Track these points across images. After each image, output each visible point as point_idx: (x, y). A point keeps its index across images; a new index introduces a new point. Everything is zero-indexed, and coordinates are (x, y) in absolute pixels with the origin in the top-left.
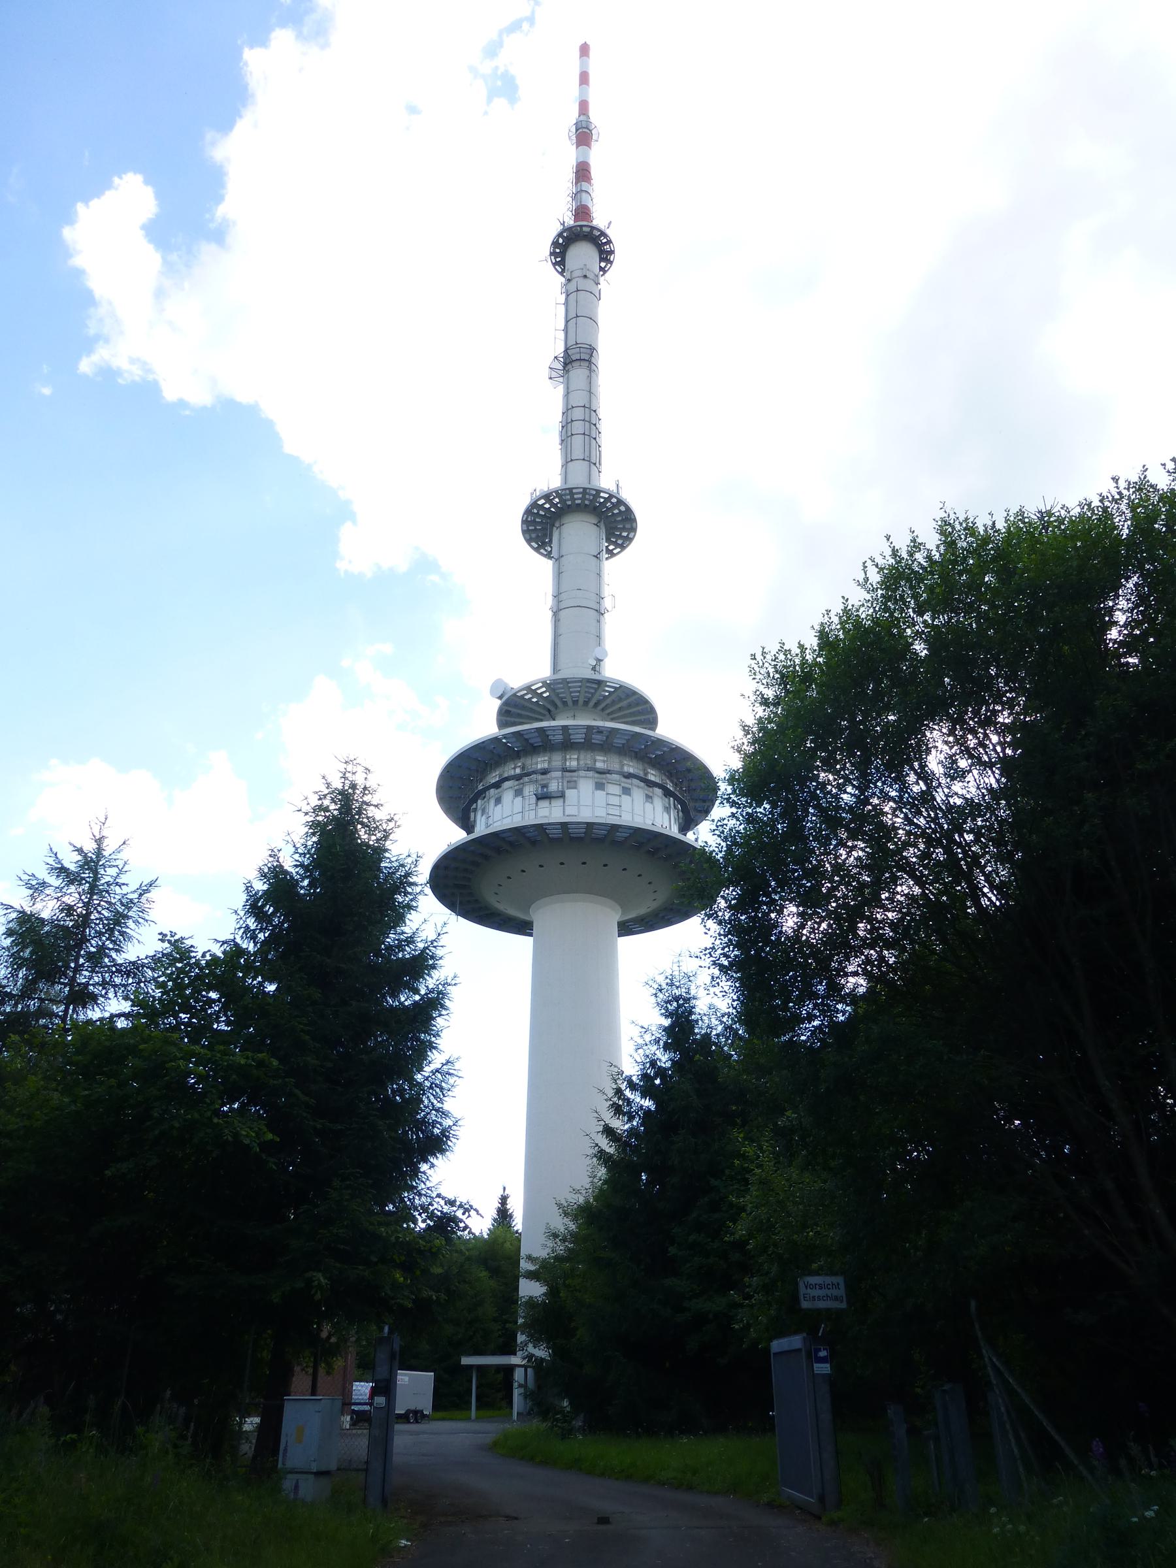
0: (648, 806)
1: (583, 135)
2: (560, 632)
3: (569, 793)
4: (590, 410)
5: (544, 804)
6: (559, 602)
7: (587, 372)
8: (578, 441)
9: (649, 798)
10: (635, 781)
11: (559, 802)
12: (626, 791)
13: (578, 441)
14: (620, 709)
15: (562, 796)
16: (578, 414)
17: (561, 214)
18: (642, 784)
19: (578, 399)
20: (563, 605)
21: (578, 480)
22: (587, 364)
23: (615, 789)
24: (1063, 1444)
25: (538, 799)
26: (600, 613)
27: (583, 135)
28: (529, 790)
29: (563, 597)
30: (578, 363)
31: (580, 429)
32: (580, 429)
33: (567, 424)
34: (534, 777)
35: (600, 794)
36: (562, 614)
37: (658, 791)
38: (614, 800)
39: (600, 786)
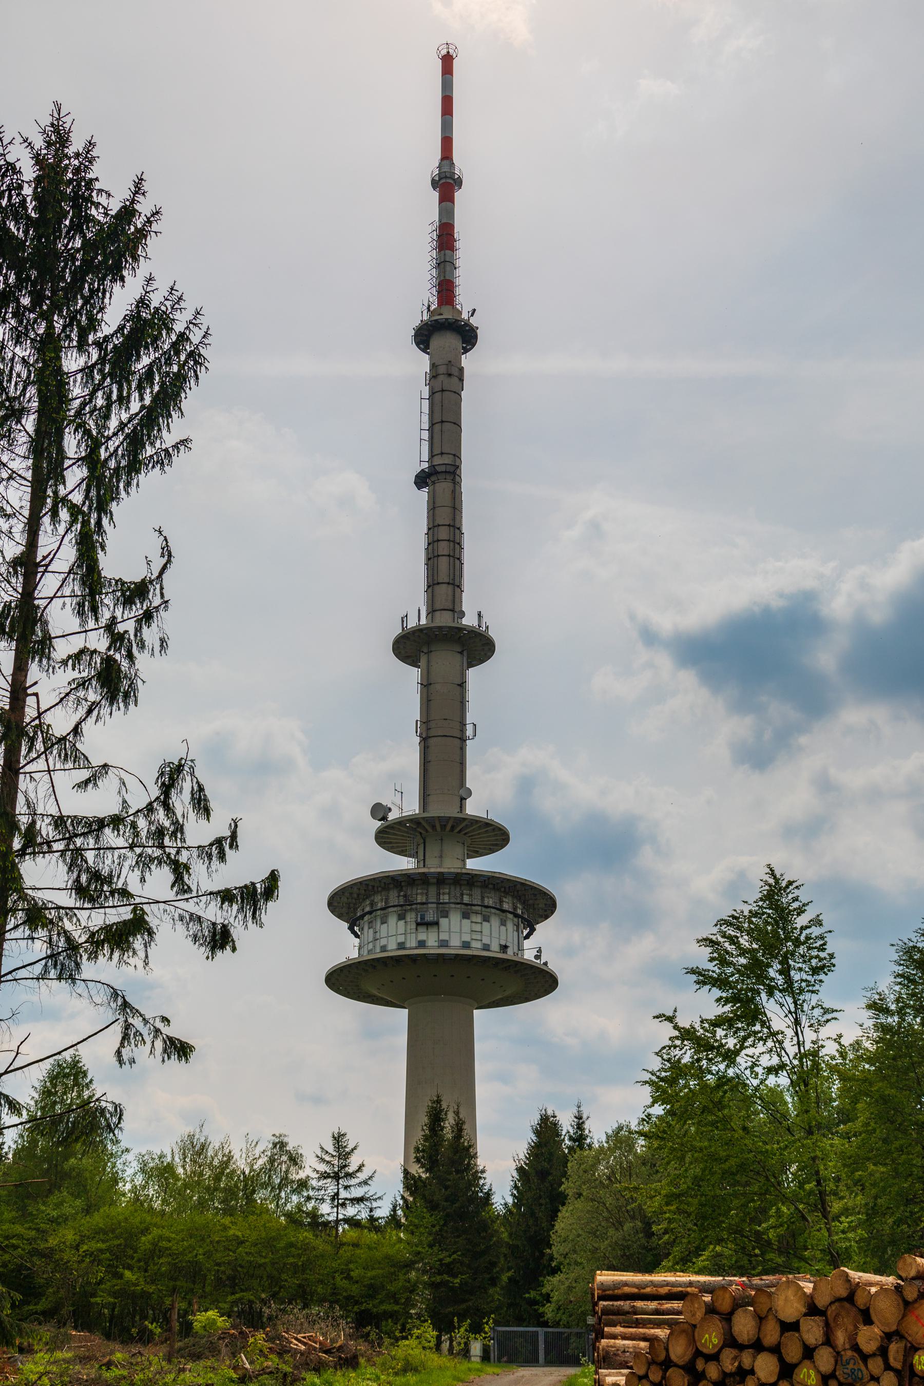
0: (503, 928)
1: (447, 184)
2: (430, 759)
3: (443, 922)
4: (455, 528)
5: (422, 929)
6: (428, 729)
7: (451, 485)
8: (443, 562)
9: (503, 923)
10: (493, 911)
11: (435, 929)
12: (486, 919)
13: (443, 562)
14: (479, 834)
15: (437, 924)
16: (443, 533)
17: (412, 605)
18: (498, 912)
19: (443, 591)
20: (432, 733)
21: (444, 620)
22: (449, 477)
23: (479, 919)
24: (713, 1279)
25: (418, 924)
26: (463, 740)
27: (447, 184)
28: (411, 917)
29: (432, 724)
30: (443, 476)
31: (446, 289)
32: (446, 289)
33: (432, 542)
34: (414, 907)
35: (466, 922)
36: (432, 741)
37: (511, 916)
38: (477, 927)
39: (466, 916)
